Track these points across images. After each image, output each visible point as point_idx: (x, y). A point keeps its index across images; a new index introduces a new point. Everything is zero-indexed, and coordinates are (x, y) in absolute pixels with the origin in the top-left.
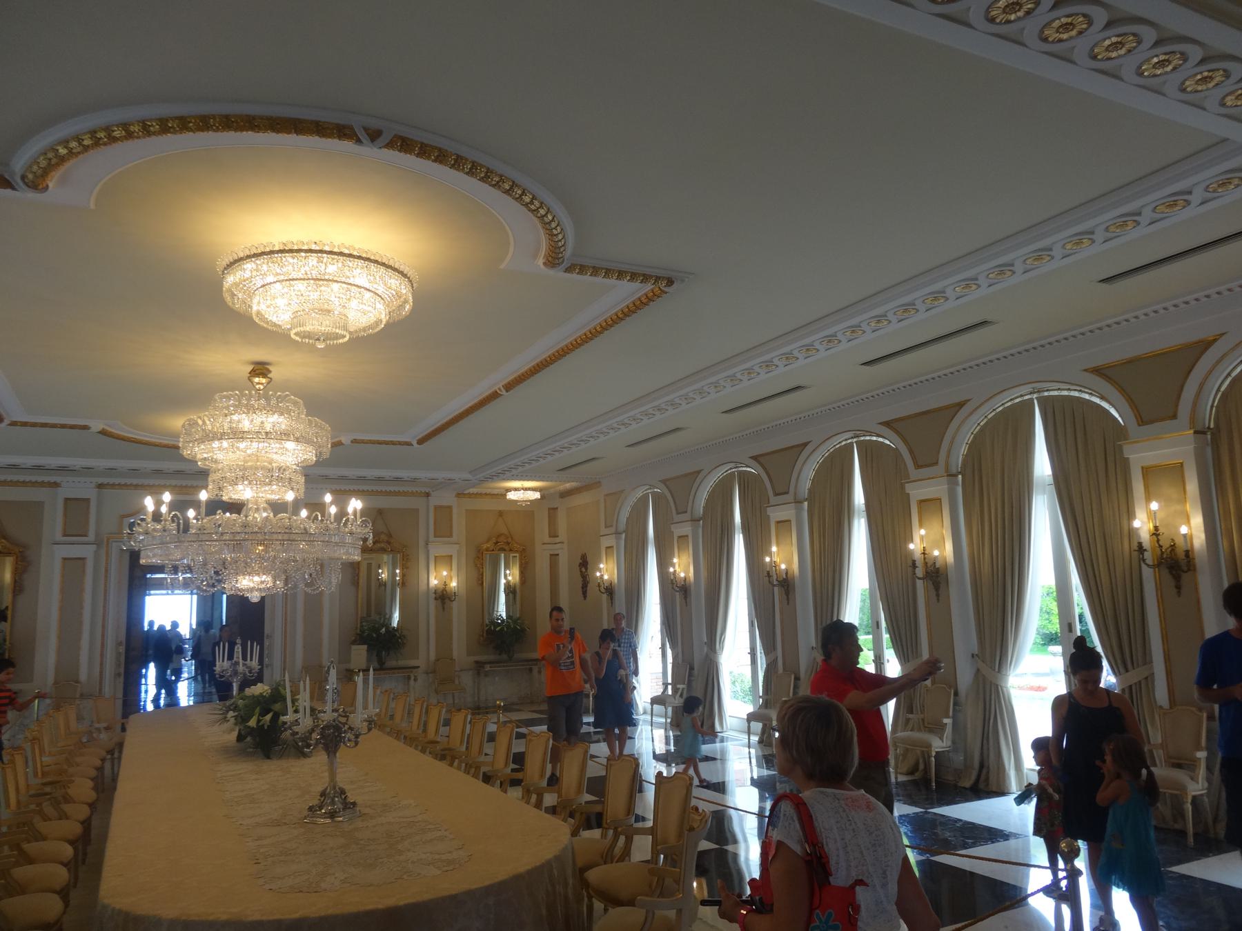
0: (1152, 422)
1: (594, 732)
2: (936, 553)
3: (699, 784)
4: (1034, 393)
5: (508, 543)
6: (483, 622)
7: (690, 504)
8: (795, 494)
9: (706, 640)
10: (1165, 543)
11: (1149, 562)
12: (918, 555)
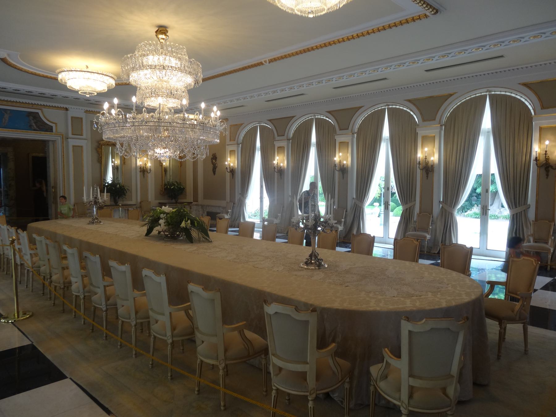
0: (548, 108)
2: (345, 162)
4: (488, 92)
6: (101, 184)
8: (287, 136)
9: (240, 193)
11: (276, 171)
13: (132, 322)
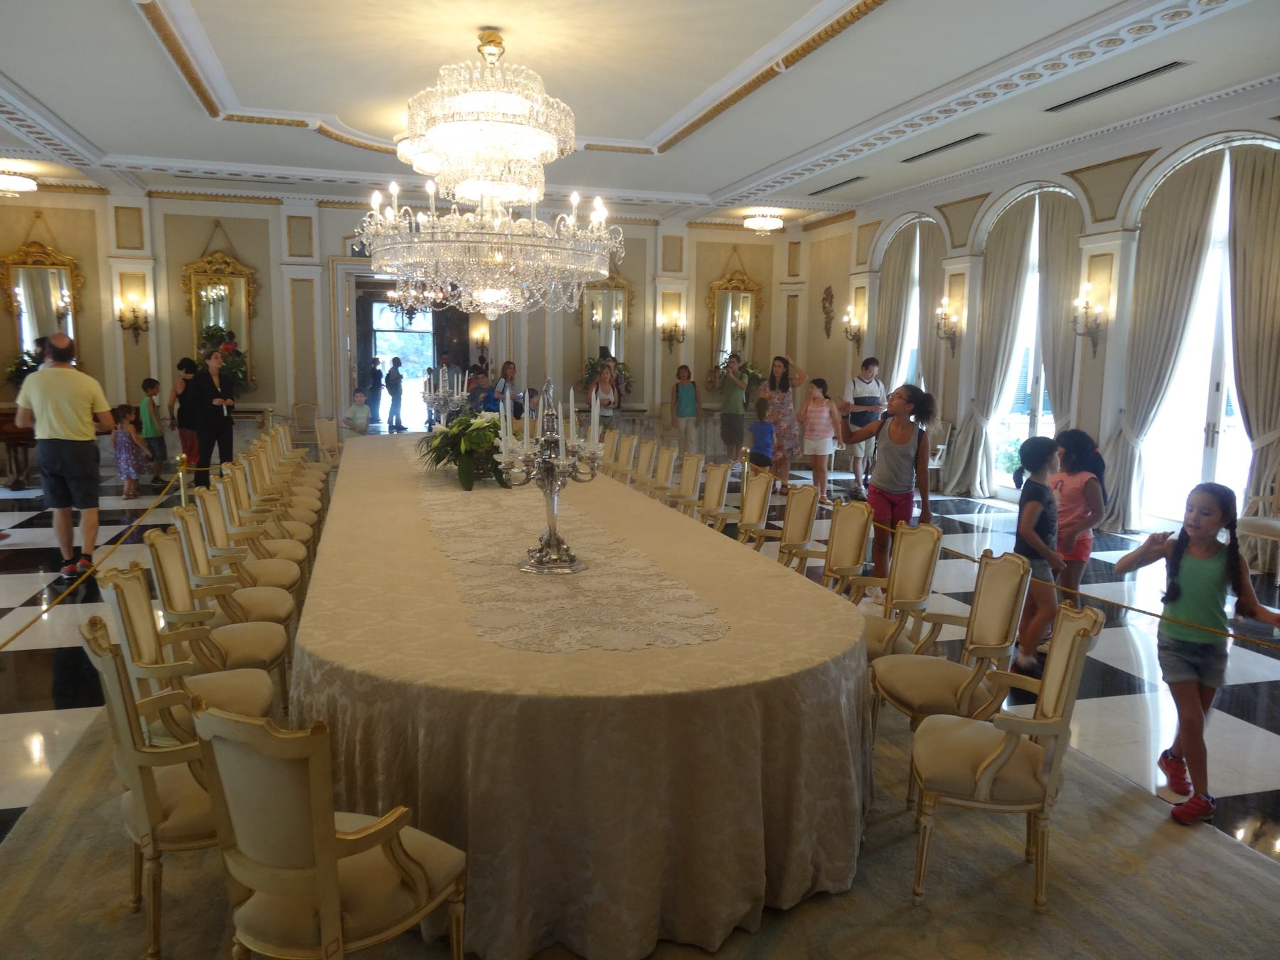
5: (743, 281)
7: (870, 255)
10: (1090, 320)
12: (1081, 310)
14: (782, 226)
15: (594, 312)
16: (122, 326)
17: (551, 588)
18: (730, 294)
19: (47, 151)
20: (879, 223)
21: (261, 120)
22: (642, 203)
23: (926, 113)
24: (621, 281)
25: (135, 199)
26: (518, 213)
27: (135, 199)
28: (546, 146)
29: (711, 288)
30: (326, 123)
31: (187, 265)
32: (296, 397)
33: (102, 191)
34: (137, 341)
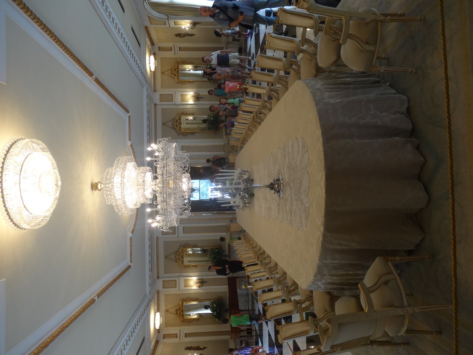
1: (255, 32)
3: (97, 190)
5: (175, 69)
13: (408, 313)
14: (153, 56)
15: (189, 119)
16: (202, 287)
17: (287, 192)
18: (180, 72)
19: (146, 312)
20: (149, 17)
21: (131, 252)
22: (149, 135)
23: (105, 11)
24: (177, 117)
25: (160, 283)
26: (156, 178)
27: (160, 283)
28: (131, 166)
29: (178, 82)
30: (129, 231)
31: (181, 267)
32: (223, 232)
33: (158, 292)
34: (206, 282)
